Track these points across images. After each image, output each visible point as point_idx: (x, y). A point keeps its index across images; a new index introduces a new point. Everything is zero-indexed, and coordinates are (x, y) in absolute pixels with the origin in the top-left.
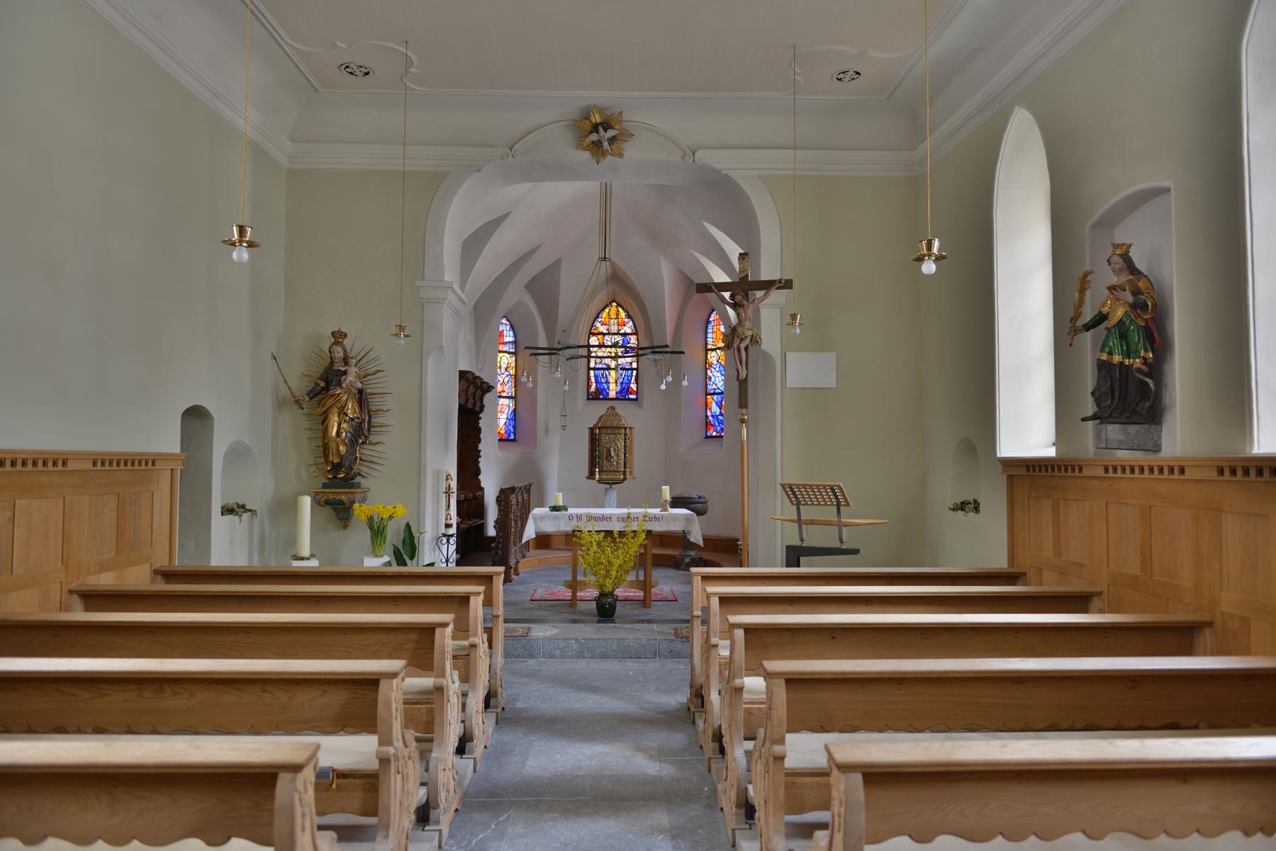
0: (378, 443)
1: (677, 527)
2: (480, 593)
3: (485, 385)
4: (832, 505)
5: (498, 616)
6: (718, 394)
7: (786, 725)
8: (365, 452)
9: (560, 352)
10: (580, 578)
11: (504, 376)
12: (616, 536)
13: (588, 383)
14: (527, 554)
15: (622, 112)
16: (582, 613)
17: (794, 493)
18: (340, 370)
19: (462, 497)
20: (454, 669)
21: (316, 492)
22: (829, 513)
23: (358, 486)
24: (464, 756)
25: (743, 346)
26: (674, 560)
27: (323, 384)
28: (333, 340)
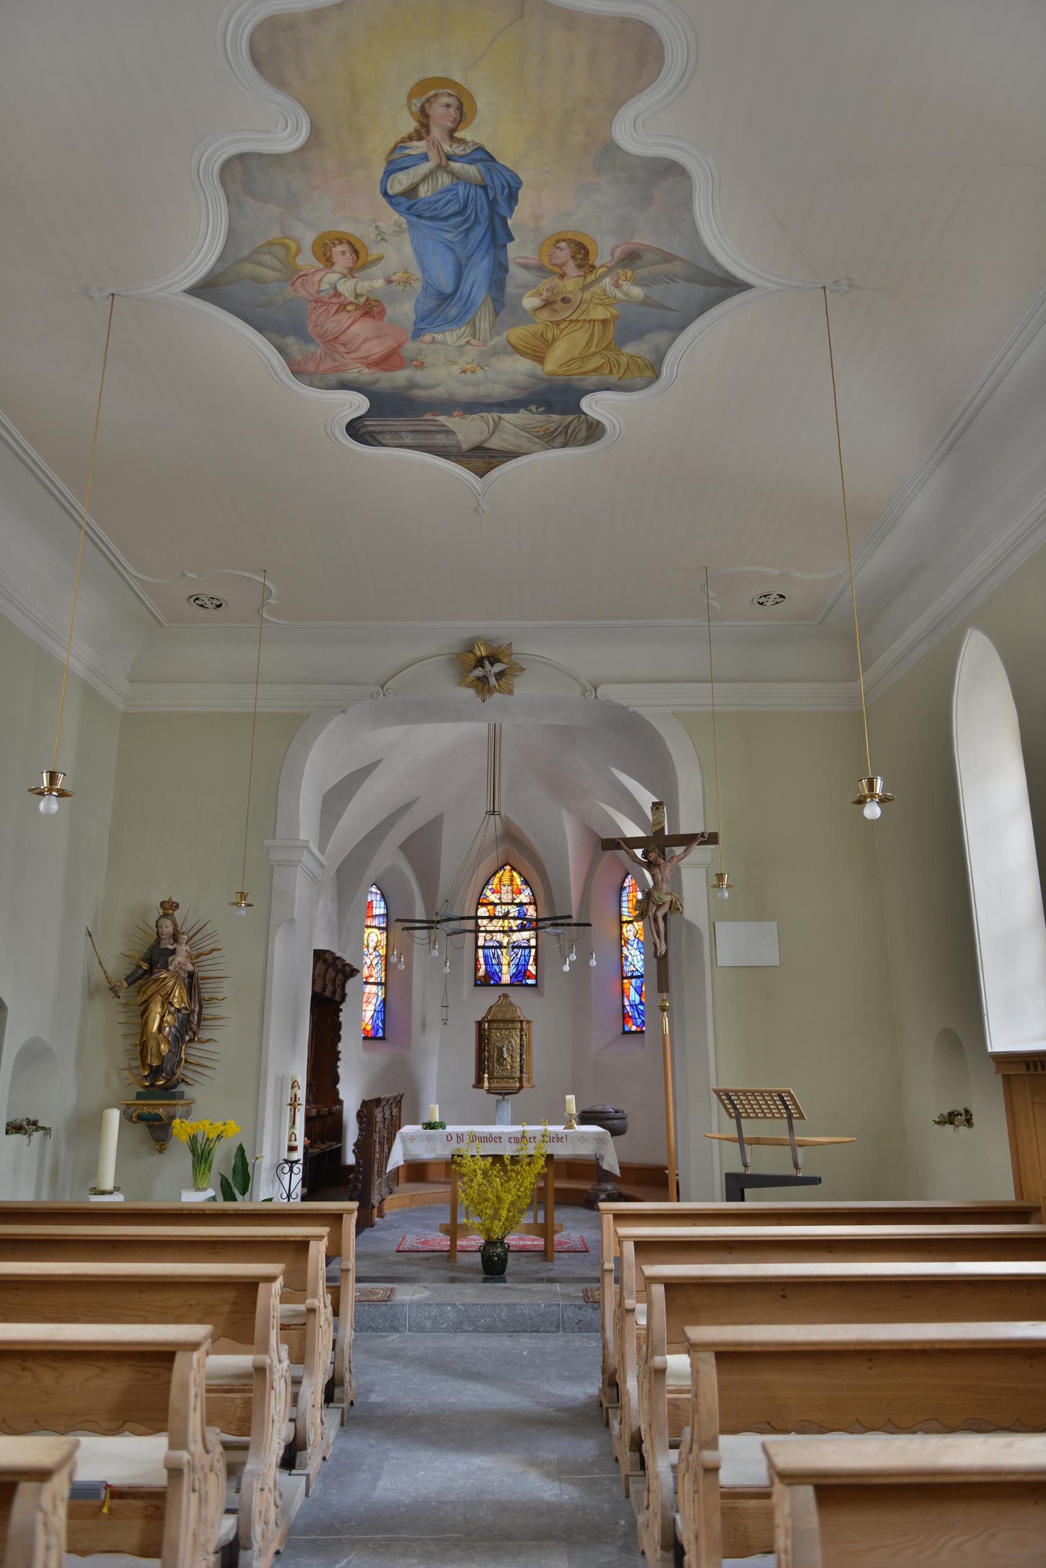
0: (209, 1040)
1: (585, 1150)
2: (323, 1237)
3: (347, 968)
4: (782, 1117)
5: (348, 1270)
6: (637, 977)
7: (718, 1420)
8: (192, 1052)
9: (439, 926)
10: (462, 1220)
11: (372, 957)
12: (507, 1162)
13: (476, 965)
14: (396, 1189)
15: (511, 644)
16: (462, 1269)
17: (732, 1102)
18: (168, 949)
19: (314, 1112)
20: (282, 1342)
21: (127, 1105)
22: (778, 1128)
23: (181, 1095)
24: (294, 1472)
25: (660, 915)
26: (586, 1196)
27: (145, 966)
28: (161, 912)
